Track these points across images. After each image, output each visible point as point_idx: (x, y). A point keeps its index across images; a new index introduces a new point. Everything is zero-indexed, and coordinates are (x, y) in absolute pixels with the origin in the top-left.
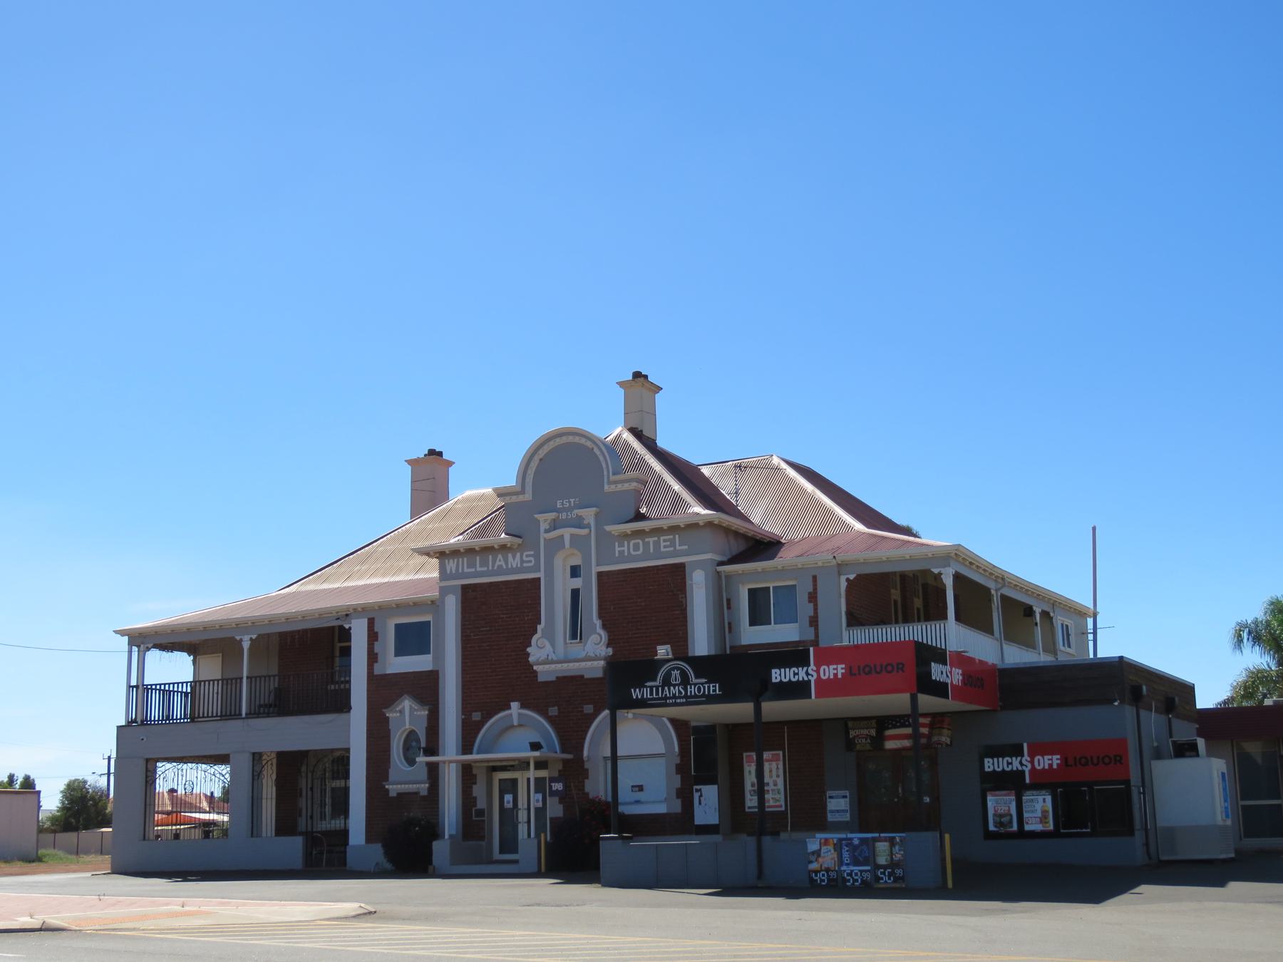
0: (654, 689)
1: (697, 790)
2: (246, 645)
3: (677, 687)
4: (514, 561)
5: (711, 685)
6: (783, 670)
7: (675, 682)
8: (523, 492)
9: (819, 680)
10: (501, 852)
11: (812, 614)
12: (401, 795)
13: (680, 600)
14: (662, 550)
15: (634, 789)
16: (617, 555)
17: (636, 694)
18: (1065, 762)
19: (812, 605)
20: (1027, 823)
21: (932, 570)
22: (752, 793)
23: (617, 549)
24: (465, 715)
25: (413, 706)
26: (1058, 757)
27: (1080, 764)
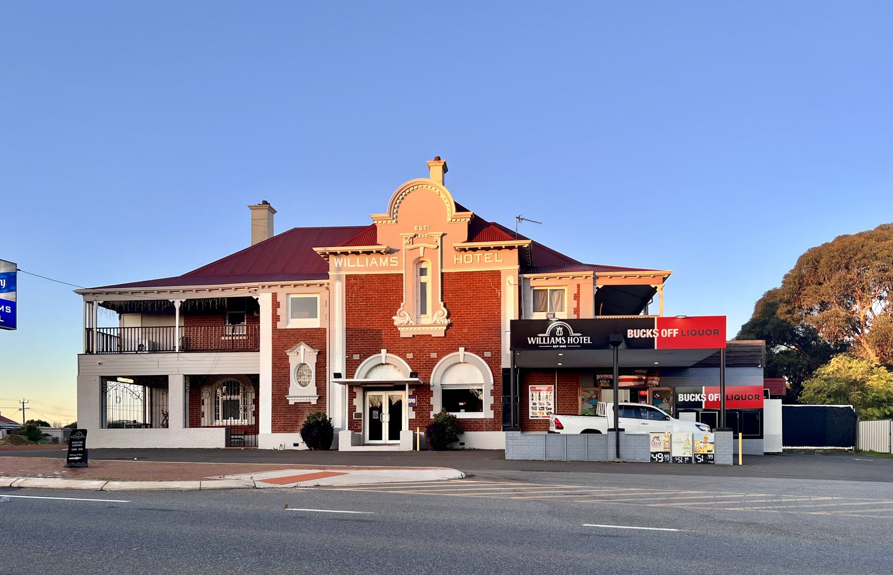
2: (177, 305)
6: (635, 330)
7: (558, 335)
9: (660, 337)
10: (370, 439)
11: (576, 307)
14: (486, 261)
16: (3, 321)
17: (531, 341)
19: (576, 301)
21: (651, 285)
23: (455, 259)
25: (307, 349)
26: (677, 330)
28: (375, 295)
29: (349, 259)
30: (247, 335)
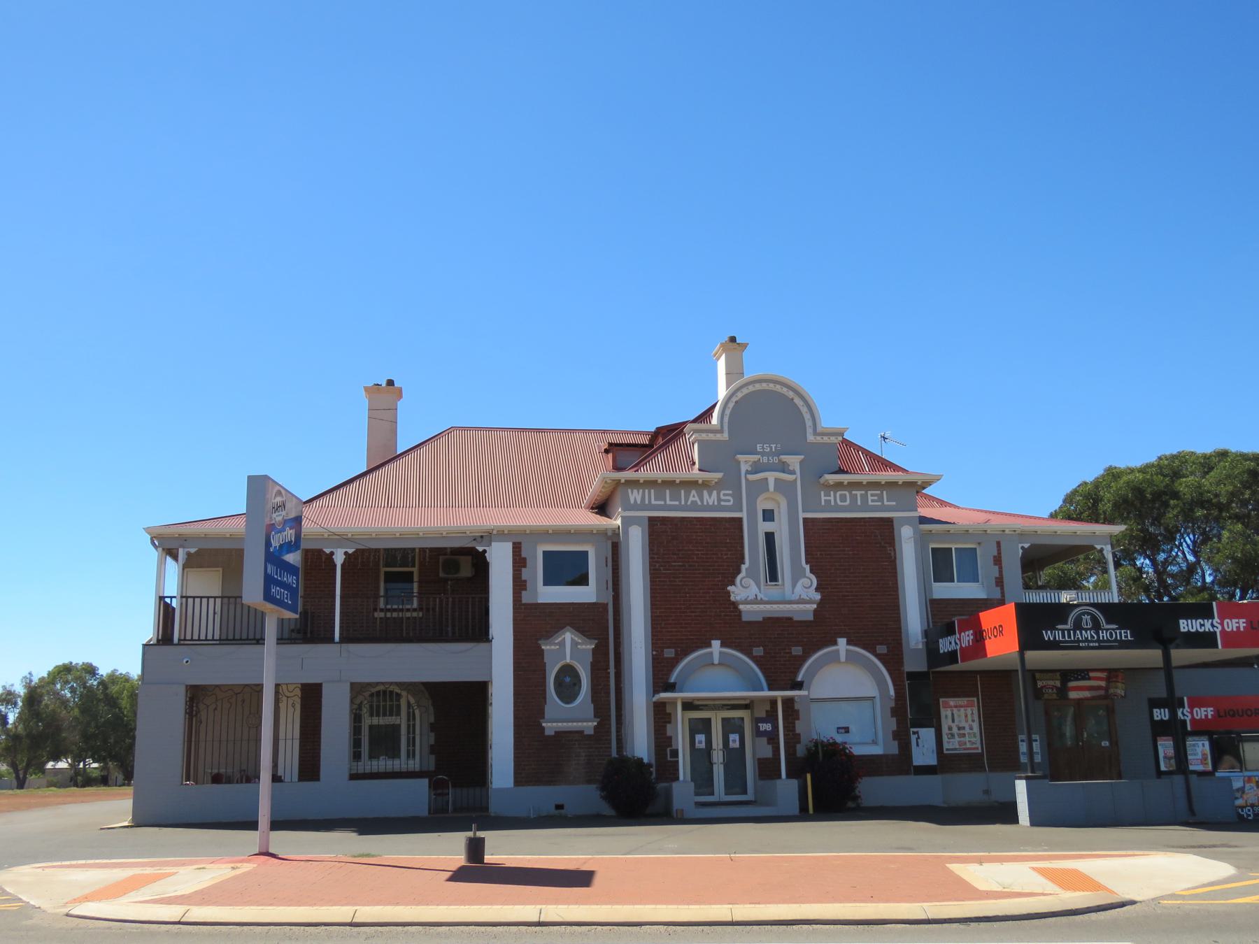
0: (1066, 632)
1: (914, 733)
2: (339, 559)
3: (1088, 632)
4: (710, 498)
5: (1123, 631)
7: (1085, 627)
8: (815, 433)
9: (1223, 632)
12: (559, 734)
13: (889, 552)
14: (870, 503)
15: (841, 730)
16: (823, 503)
17: (1048, 635)
18: (1218, 714)
19: (997, 567)
20: (1191, 764)
22: (949, 736)
23: (823, 498)
24: (656, 651)
25: (576, 639)
26: (1244, 620)
27: (1246, 714)
28: (698, 550)
29: (652, 491)
30: (421, 609)
